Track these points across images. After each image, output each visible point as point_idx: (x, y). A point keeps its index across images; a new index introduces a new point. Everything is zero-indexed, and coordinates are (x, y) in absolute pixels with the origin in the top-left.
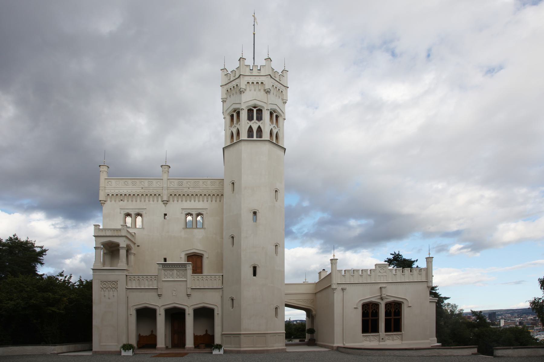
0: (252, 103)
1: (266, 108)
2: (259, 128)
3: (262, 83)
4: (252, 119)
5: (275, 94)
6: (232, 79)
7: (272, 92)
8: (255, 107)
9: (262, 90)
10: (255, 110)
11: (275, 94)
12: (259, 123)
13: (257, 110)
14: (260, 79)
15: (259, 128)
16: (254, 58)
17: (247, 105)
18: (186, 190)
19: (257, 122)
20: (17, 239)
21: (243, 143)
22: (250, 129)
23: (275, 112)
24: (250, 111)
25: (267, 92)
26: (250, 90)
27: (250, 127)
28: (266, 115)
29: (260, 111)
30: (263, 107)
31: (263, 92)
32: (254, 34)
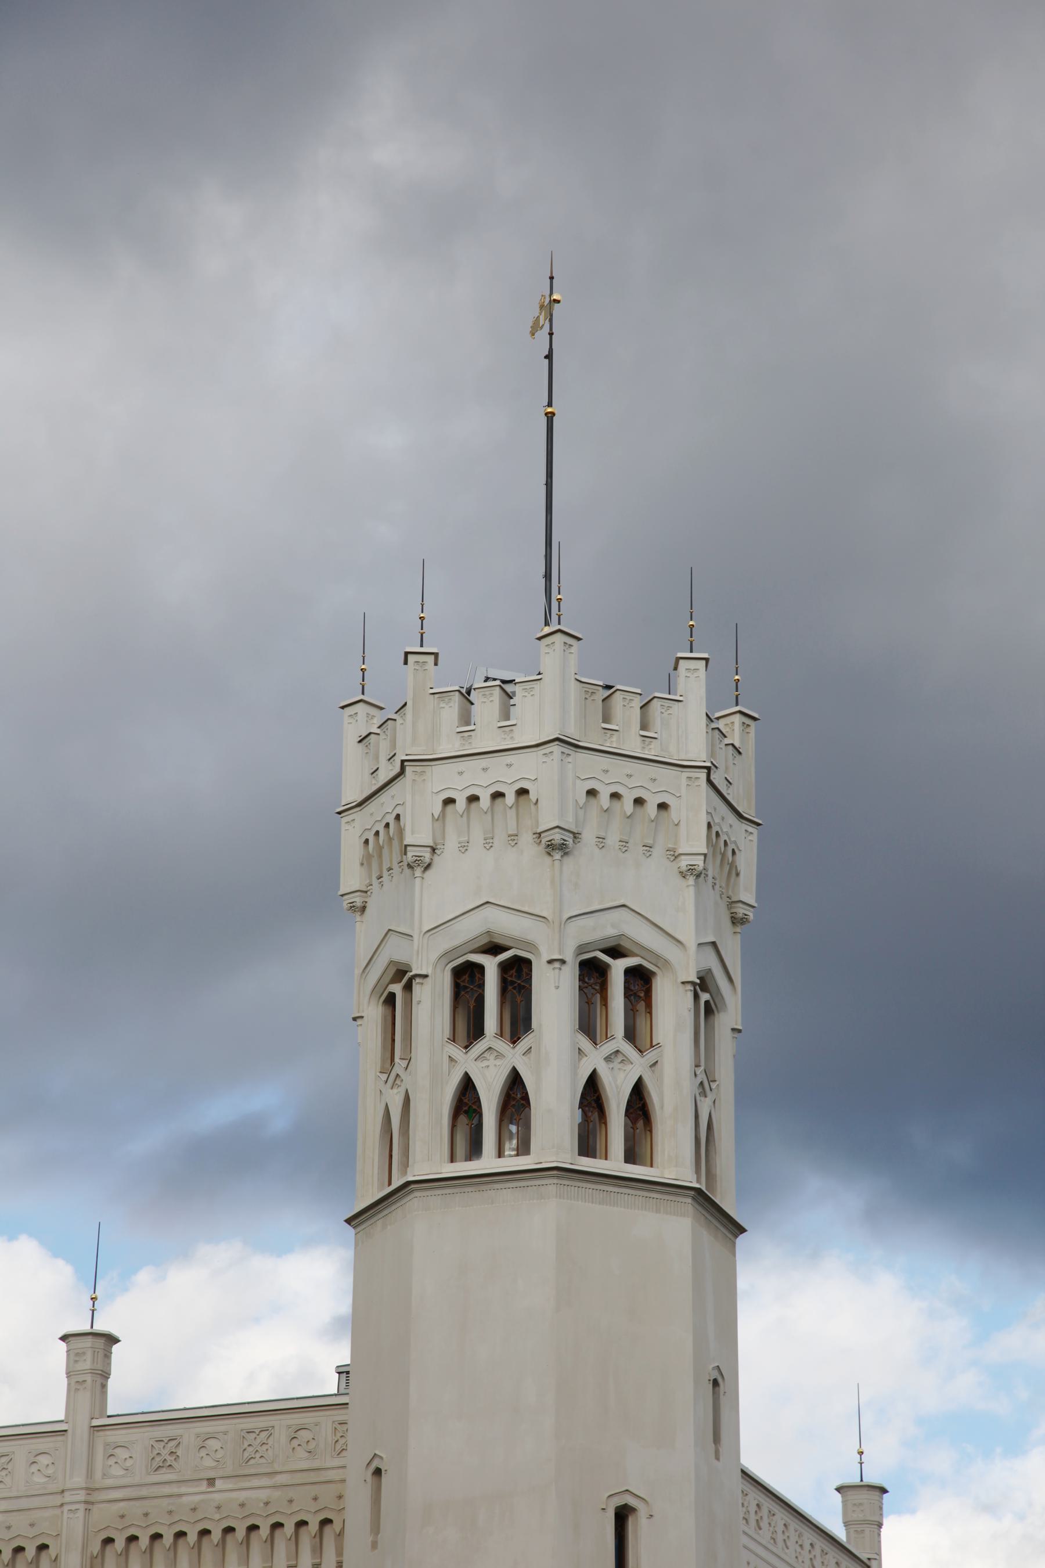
0: (471, 929)
1: (546, 957)
2: (515, 1081)
3: (523, 792)
4: (476, 1031)
5: (613, 839)
6: (383, 777)
7: (588, 836)
8: (493, 949)
9: (527, 838)
10: (491, 965)
11: (613, 839)
12: (513, 1056)
13: (505, 968)
14: (506, 774)
15: (515, 1081)
16: (548, 576)
17: (446, 942)
18: (194, 1495)
19: (502, 1046)
20: (338, 1322)
21: (415, 1203)
22: (466, 1100)
23: (616, 952)
24: (466, 978)
25: (559, 846)
26: (464, 848)
27: (467, 1086)
28: (554, 996)
29: (517, 974)
30: (531, 946)
31: (530, 850)
32: (550, 417)
